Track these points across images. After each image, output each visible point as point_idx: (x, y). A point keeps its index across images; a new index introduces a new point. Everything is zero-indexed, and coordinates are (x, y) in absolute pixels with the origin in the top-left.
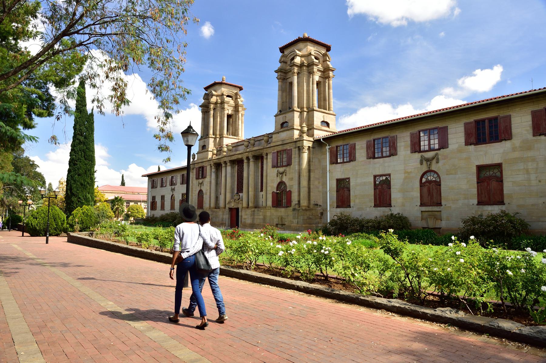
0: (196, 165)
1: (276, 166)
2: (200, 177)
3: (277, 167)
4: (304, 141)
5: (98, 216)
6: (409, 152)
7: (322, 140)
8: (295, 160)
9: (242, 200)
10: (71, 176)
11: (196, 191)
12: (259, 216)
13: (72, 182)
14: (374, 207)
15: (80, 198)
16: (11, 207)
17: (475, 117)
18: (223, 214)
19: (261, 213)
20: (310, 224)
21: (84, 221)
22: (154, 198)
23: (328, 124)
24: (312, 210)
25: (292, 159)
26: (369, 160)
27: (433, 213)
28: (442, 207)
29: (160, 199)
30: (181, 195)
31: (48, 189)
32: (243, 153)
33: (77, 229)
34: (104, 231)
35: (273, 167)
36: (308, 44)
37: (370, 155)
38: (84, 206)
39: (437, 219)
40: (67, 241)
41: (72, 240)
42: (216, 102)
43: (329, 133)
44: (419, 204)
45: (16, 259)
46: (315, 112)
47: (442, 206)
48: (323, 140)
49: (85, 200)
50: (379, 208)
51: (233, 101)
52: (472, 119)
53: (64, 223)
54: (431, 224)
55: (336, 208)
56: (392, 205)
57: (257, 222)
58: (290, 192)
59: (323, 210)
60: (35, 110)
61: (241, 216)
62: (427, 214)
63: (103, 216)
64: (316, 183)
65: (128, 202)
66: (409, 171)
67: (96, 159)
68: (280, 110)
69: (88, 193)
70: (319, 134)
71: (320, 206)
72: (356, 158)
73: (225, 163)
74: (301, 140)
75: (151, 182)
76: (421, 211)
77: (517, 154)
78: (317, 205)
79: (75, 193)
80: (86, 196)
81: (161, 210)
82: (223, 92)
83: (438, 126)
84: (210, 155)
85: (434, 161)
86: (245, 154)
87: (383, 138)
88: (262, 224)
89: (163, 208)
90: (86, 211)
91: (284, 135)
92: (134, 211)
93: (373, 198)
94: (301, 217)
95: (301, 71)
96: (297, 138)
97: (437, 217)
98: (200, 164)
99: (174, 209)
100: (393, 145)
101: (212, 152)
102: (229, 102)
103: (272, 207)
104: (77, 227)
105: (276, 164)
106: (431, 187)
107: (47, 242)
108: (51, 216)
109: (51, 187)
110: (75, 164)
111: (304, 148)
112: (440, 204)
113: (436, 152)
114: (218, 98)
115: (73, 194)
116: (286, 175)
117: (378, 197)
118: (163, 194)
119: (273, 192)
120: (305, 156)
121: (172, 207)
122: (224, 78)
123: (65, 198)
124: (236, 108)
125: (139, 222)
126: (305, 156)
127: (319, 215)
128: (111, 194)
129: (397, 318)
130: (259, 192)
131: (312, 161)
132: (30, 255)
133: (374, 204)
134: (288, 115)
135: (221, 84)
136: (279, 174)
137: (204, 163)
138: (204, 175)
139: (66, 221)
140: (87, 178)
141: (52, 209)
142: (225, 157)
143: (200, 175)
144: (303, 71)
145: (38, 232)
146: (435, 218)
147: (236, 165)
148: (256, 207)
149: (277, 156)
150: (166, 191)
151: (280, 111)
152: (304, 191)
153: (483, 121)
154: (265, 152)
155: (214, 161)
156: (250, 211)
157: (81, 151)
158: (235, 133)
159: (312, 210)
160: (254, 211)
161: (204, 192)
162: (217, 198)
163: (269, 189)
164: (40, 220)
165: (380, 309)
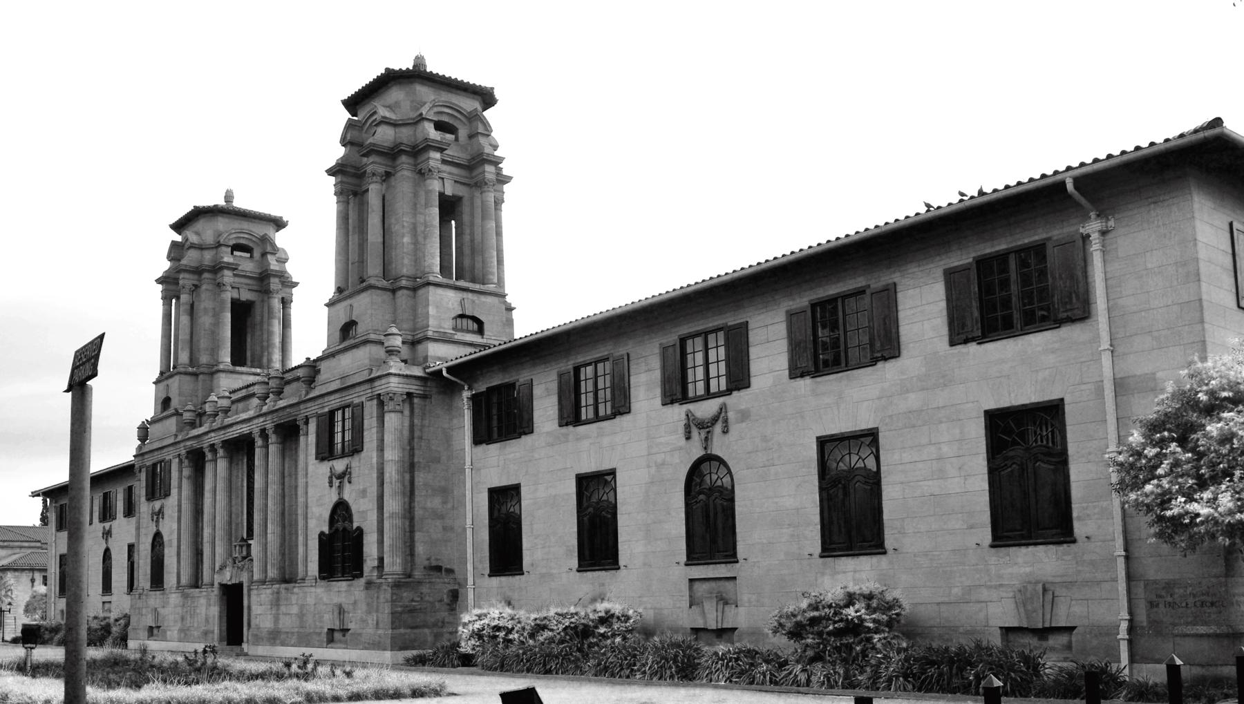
0: (146, 456)
6: (658, 401)
7: (445, 373)
9: (252, 560)
17: (853, 281)
18: (209, 605)
20: (412, 628)
24: (420, 583)
25: (365, 433)
26: (564, 430)
39: (726, 603)
46: (431, 288)
47: (737, 562)
48: (1076, 187)
52: (962, 257)
55: (490, 576)
58: (360, 531)
61: (249, 608)
62: (705, 586)
71: (450, 571)
73: (212, 446)
76: (691, 581)
77: (914, 400)
78: (438, 569)
83: (724, 321)
85: (718, 428)
86: (256, 421)
87: (596, 362)
88: (296, 630)
93: (575, 542)
98: (156, 453)
106: (711, 502)
113: (721, 400)
116: (350, 482)
119: (322, 534)
131: (421, 438)
137: (165, 450)
144: (399, 168)
146: (722, 599)
148: (285, 580)
151: (339, 290)
153: (1002, 257)
156: (269, 591)
161: (166, 538)
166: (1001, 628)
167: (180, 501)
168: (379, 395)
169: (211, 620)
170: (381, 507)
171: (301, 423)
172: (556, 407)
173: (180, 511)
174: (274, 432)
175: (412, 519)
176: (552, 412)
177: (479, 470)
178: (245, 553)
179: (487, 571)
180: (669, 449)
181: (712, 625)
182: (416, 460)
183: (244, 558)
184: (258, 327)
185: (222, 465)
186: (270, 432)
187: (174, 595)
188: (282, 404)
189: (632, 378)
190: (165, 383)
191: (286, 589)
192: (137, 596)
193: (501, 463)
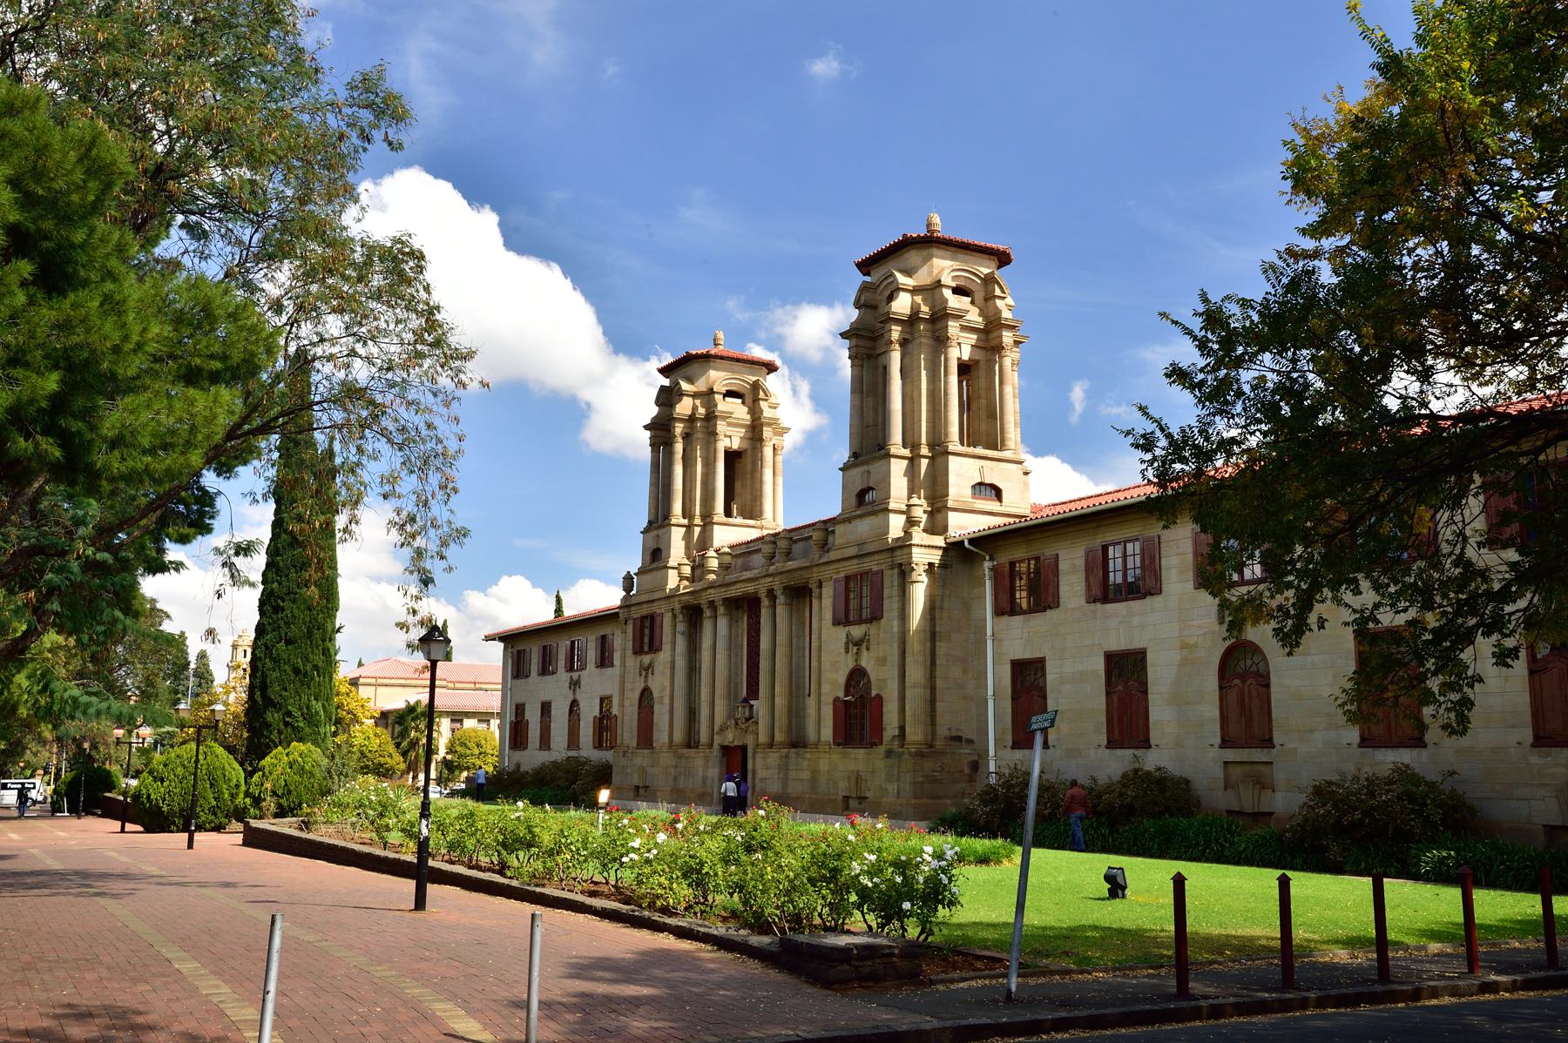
0: (633, 608)
1: (844, 620)
2: (646, 648)
3: (847, 623)
4: (914, 550)
5: (329, 772)
6: (1190, 585)
7: (966, 544)
8: (891, 606)
9: (757, 723)
10: (266, 645)
11: (633, 690)
12: (801, 772)
13: (269, 663)
14: (1107, 747)
15: (289, 714)
16: (86, 745)
18: (706, 766)
19: (805, 764)
21: (292, 788)
22: (520, 709)
23: (997, 493)
24: (943, 753)
25: (885, 602)
26: (1092, 606)
27: (1255, 766)
28: (1274, 751)
29: (539, 714)
30: (598, 700)
31: (196, 670)
32: (757, 578)
33: (268, 810)
34: (335, 816)
35: (837, 622)
36: (935, 251)
37: (1094, 592)
38: (294, 744)
39: (1264, 788)
40: (241, 843)
41: (256, 839)
42: (690, 416)
43: (1000, 521)
44: (1218, 741)
45: (126, 876)
46: (950, 457)
47: (1274, 747)
48: (969, 544)
49: (305, 719)
50: (1119, 752)
51: (746, 409)
53: (237, 794)
54: (1247, 800)
55: (1012, 748)
56: (1153, 742)
57: (794, 789)
58: (879, 699)
59: (979, 755)
60: (170, 530)
61: (754, 772)
63: (341, 774)
64: (956, 672)
65: (457, 717)
66: (1192, 641)
67: (340, 590)
68: (854, 453)
69: (316, 699)
70: (962, 525)
71: (970, 742)
72: (1061, 600)
73: (712, 604)
74: (904, 544)
75: (512, 657)
76: (1225, 762)
78: (959, 739)
79: (277, 699)
80: (308, 708)
81: (541, 748)
82: (714, 383)
84: (673, 580)
86: (763, 581)
88: (807, 796)
89: (545, 742)
90: (300, 759)
91: (863, 527)
92: (468, 752)
94: (908, 775)
95: (912, 334)
96: (898, 539)
97: (1263, 784)
98: (645, 606)
99: (578, 748)
100: (1150, 563)
101: (676, 571)
102: (732, 413)
103: (835, 743)
104: (270, 804)
105: (842, 615)
106: (1246, 689)
107: (190, 846)
108: (204, 772)
109: (206, 665)
110: (277, 609)
111: (913, 569)
112: (1268, 743)
114: (698, 402)
115: (269, 703)
116: (868, 649)
117: (1115, 718)
118: (546, 698)
119: (836, 700)
120: (919, 593)
121: (573, 740)
122: (721, 335)
123: (247, 713)
124: (755, 431)
125: (481, 791)
126: (919, 593)
127: (967, 771)
128: (401, 689)
129: (606, 925)
130: (804, 697)
131: (942, 608)
132: (154, 871)
133: (1108, 740)
134: (875, 467)
135: (706, 358)
136: (851, 646)
138: (656, 644)
139: (243, 788)
140: (312, 653)
141: (205, 753)
142: (712, 587)
143: (646, 640)
145: (166, 818)
146: (1258, 783)
147: (743, 612)
149: (847, 590)
150: (554, 688)
151: (855, 455)
152: (915, 697)
154: (815, 575)
155: (683, 598)
156: (777, 755)
157: (295, 566)
158: (752, 507)
159: (943, 753)
160: (787, 756)
161: (656, 695)
162: (692, 714)
163: (826, 688)
164: (173, 784)
165: (662, 931)
166: (1544, 826)
167: (673, 656)
168: (901, 565)
169: (709, 781)
170: (902, 675)
171: (813, 586)
172: (1084, 584)
173: (673, 667)
174: (782, 594)
175: (933, 689)
176: (1079, 588)
177: (1000, 641)
178: (747, 714)
179: (1010, 743)
180: (1201, 632)
181: (1249, 809)
182: (937, 629)
183: (747, 720)
184: (749, 476)
185: (722, 623)
186: (778, 593)
187: (665, 755)
188: (791, 565)
189: (1163, 560)
190: (654, 533)
191: (797, 753)
192: (621, 754)
193: (1025, 636)
